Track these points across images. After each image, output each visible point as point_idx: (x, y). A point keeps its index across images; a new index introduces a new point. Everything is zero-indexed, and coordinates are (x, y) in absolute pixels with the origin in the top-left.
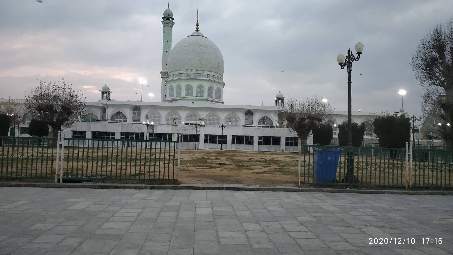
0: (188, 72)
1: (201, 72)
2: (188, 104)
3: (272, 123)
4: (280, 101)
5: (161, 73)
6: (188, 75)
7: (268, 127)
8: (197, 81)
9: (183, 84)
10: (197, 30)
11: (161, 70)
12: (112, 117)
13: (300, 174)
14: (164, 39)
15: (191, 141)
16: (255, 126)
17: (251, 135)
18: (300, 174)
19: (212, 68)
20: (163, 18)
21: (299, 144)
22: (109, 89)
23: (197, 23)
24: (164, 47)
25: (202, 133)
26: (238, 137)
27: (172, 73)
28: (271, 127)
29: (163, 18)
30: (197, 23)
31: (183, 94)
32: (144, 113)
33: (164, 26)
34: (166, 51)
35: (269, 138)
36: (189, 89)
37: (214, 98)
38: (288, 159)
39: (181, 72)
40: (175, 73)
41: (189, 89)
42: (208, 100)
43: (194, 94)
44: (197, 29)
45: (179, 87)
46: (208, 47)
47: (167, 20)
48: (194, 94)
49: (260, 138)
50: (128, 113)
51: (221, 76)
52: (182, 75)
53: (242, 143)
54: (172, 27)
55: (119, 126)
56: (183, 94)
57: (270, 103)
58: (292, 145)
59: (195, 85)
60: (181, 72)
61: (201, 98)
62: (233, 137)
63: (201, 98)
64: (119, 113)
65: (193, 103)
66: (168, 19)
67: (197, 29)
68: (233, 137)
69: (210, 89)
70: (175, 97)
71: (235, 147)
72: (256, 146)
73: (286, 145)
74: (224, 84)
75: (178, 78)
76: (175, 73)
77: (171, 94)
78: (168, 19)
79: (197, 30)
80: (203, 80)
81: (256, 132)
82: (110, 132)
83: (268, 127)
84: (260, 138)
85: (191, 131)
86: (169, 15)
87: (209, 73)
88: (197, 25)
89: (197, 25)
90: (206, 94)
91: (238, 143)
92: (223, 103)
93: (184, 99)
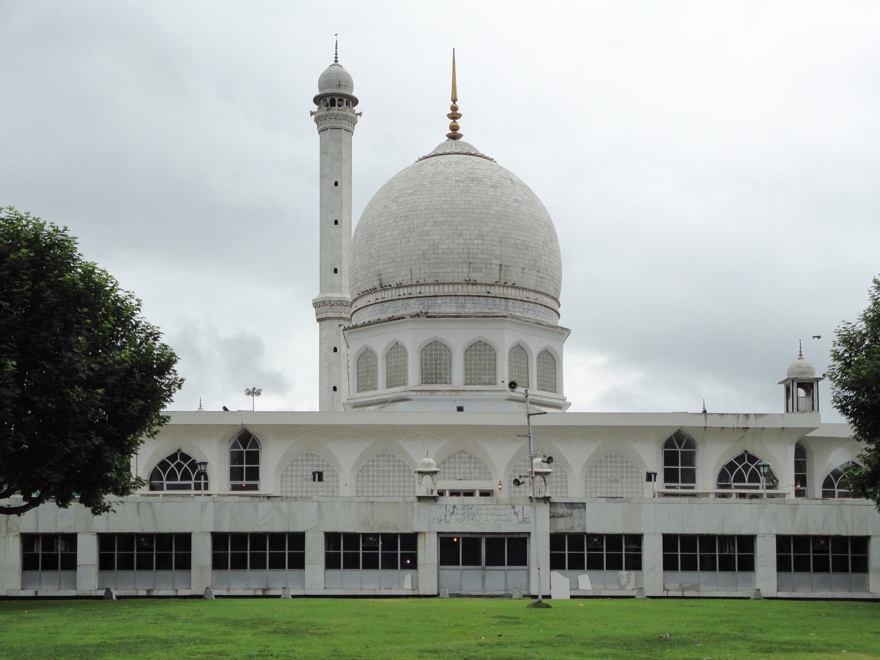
2: (439, 413)
3: (772, 480)
4: (802, 392)
5: (317, 305)
11: (315, 293)
12: (155, 475)
14: (322, 177)
15: (495, 560)
16: (707, 495)
17: (745, 531)
20: (317, 100)
21: (759, 562)
23: (454, 109)
24: (325, 205)
26: (689, 541)
29: (317, 100)
30: (454, 109)
33: (321, 131)
34: (333, 222)
44: (454, 128)
50: (217, 461)
53: (708, 566)
54: (351, 132)
55: (203, 506)
57: (175, 396)
58: (50, 564)
62: (219, 539)
64: (178, 457)
65: (460, 409)
66: (335, 102)
67: (454, 128)
68: (219, 539)
69: (519, 351)
70: (382, 391)
71: (560, 585)
72: (652, 573)
77: (365, 380)
78: (335, 102)
79: (454, 135)
81: (656, 516)
82: (395, 535)
89: (454, 115)
91: (689, 565)
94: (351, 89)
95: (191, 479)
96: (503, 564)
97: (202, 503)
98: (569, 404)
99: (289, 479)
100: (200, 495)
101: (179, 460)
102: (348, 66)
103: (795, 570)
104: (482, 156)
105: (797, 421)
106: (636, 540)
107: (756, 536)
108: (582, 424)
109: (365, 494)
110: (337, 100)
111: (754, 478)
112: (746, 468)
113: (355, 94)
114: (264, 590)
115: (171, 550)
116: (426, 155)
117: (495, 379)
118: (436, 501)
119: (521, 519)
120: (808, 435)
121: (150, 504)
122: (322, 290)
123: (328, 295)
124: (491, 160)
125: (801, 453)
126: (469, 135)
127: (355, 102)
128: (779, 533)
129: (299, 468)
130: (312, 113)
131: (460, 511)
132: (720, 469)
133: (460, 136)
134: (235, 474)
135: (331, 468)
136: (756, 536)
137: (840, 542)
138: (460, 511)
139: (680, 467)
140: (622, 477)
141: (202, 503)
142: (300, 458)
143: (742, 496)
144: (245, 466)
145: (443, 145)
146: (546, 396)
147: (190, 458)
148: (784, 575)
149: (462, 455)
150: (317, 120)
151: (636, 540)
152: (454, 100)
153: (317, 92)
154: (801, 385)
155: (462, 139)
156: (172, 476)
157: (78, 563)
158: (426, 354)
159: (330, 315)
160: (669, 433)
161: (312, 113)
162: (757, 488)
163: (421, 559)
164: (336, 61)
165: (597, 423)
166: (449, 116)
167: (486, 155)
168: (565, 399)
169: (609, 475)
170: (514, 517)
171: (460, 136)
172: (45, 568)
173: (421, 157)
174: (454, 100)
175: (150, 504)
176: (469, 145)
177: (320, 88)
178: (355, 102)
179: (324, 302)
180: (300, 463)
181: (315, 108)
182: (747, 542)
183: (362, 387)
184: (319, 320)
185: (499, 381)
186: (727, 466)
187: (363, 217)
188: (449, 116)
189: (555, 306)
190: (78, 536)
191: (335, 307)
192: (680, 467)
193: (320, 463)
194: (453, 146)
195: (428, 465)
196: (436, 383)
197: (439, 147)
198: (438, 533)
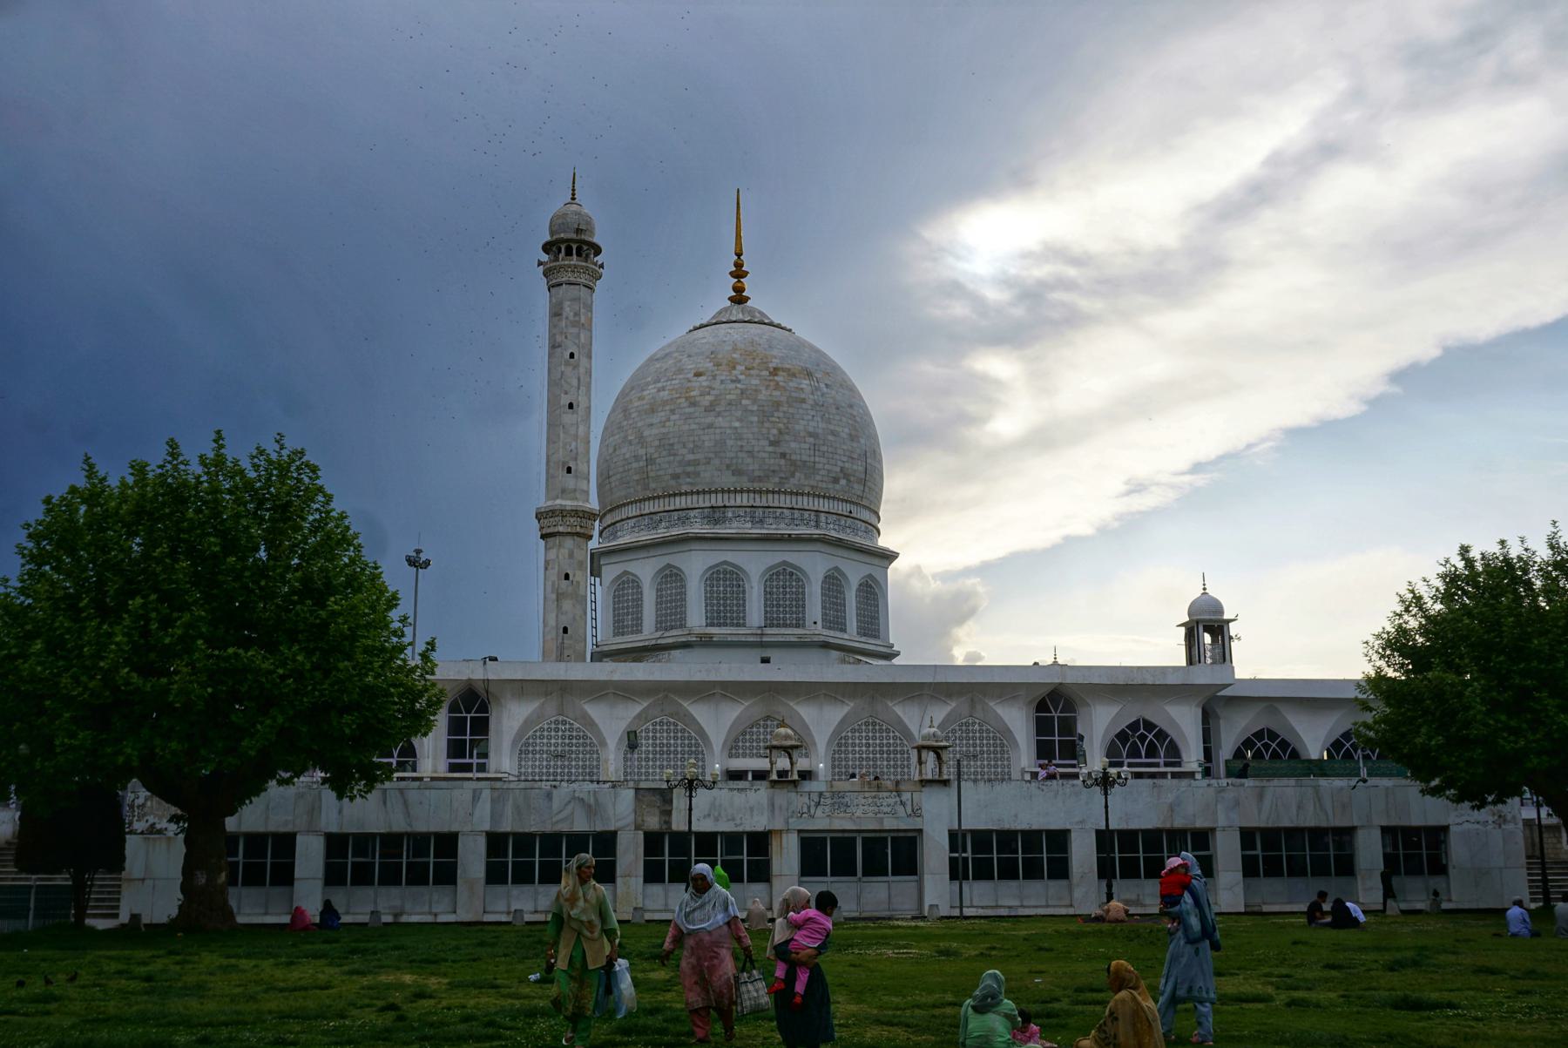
1: (786, 501)
2: (743, 668)
3: (1174, 752)
4: (1207, 638)
6: (715, 514)
7: (1163, 775)
8: (768, 546)
10: (739, 298)
15: (874, 868)
19: (836, 480)
20: (547, 248)
22: (1218, 608)
23: (739, 265)
25: (936, 819)
27: (632, 511)
28: (1174, 775)
29: (547, 248)
30: (739, 265)
31: (696, 618)
32: (509, 720)
35: (1007, 838)
36: (725, 583)
37: (851, 635)
38: (304, 972)
39: (680, 502)
40: (649, 507)
41: (725, 588)
42: (826, 646)
44: (739, 290)
45: (672, 578)
46: (809, 375)
47: (569, 253)
49: (1248, 836)
51: (865, 515)
52: (684, 521)
56: (696, 618)
59: (755, 564)
60: (680, 502)
63: (791, 634)
65: (765, 661)
67: (739, 290)
69: (833, 583)
70: (648, 632)
72: (936, 888)
73: (954, 876)
74: (889, 556)
75: (662, 532)
76: (649, 507)
79: (739, 298)
80: (799, 539)
83: (1163, 775)
84: (1248, 836)
85: (864, 814)
86: (578, 231)
87: (824, 505)
88: (739, 273)
89: (739, 273)
90: (814, 609)
94: (592, 233)
96: (886, 874)
97: (475, 791)
98: (897, 654)
102: (589, 206)
103: (1265, 875)
104: (778, 326)
105: (1204, 675)
106: (1345, 834)
107: (1213, 830)
108: (865, 680)
111: (1152, 751)
112: (1143, 738)
113: (596, 240)
114: (396, 915)
115: (506, 856)
116: (704, 322)
119: (909, 811)
120: (1222, 693)
121: (401, 791)
125: (1208, 717)
126: (757, 300)
127: (598, 251)
128: (1245, 825)
130: (540, 263)
131: (829, 801)
132: (1108, 741)
136: (1213, 830)
137: (1031, 838)
138: (829, 801)
140: (982, 752)
141: (475, 791)
143: (1138, 776)
145: (726, 309)
146: (871, 645)
148: (1253, 881)
151: (1345, 834)
152: (739, 255)
154: (1207, 629)
157: (297, 875)
159: (561, 529)
160: (1043, 692)
161: (540, 263)
162: (1157, 765)
163: (776, 868)
165: (928, 679)
170: (900, 809)
172: (355, 882)
174: (739, 255)
175: (401, 791)
177: (552, 233)
178: (598, 251)
181: (545, 257)
182: (1059, 840)
183: (619, 628)
185: (809, 622)
187: (622, 405)
189: (873, 520)
190: (299, 838)
195: (787, 737)
197: (720, 313)
198: (799, 831)
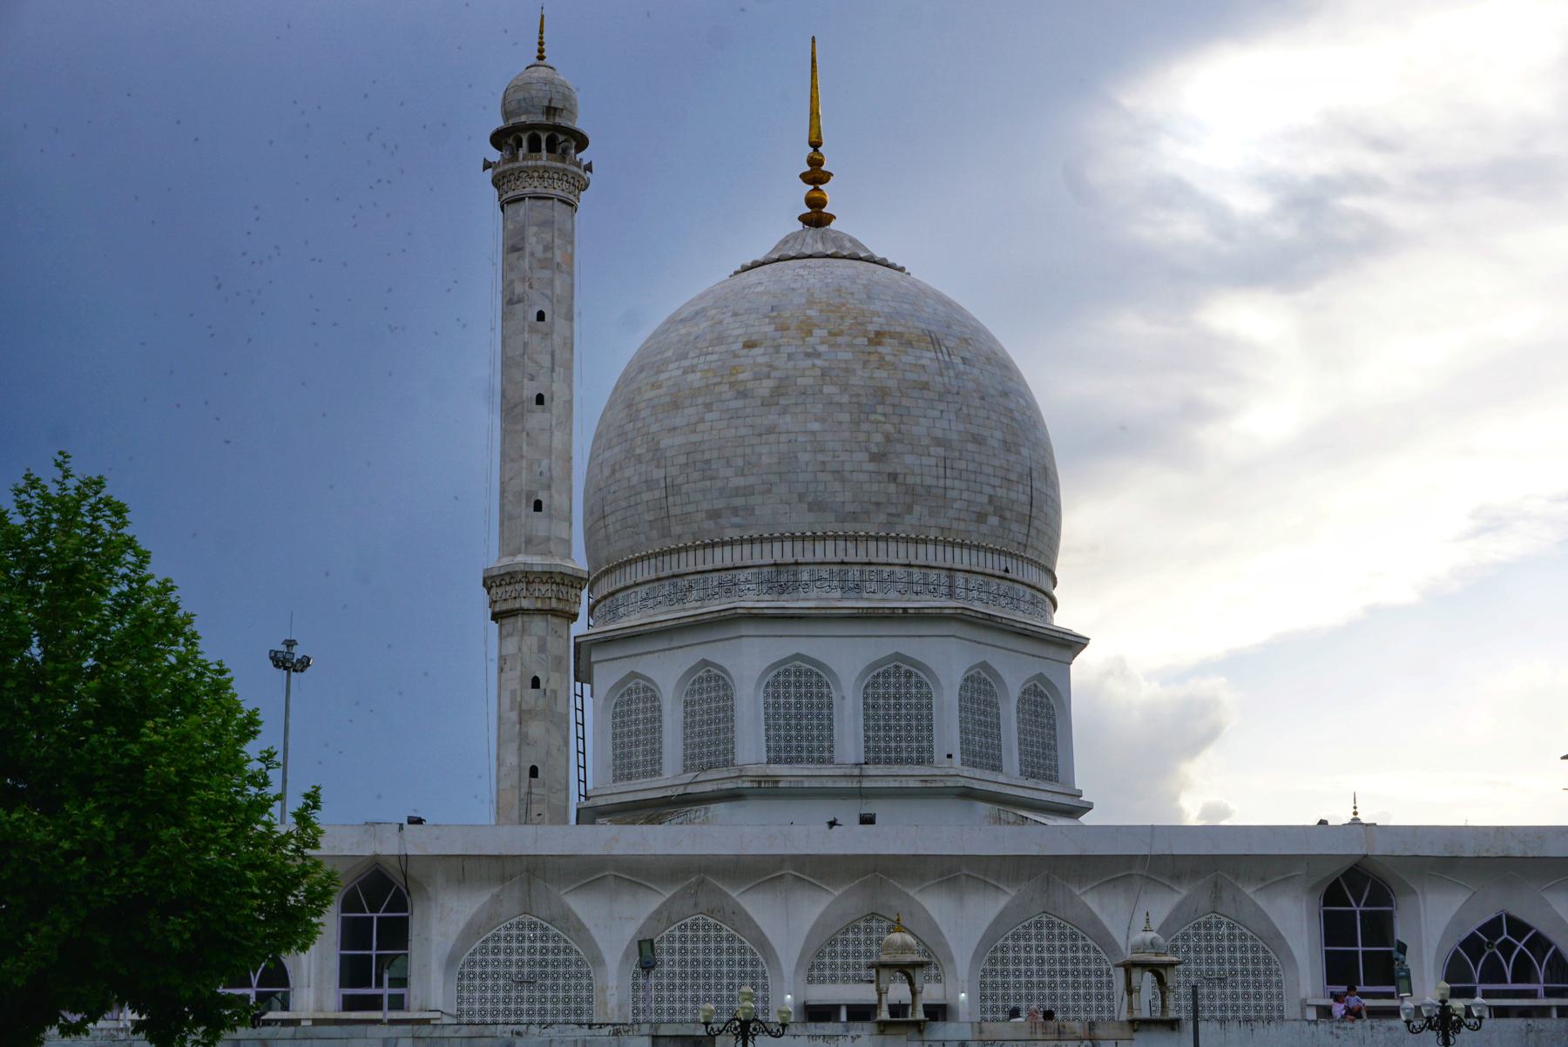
0: (779, 553)
2: (800, 832)
6: (781, 576)
7: (1543, 1012)
8: (870, 629)
9: (749, 661)
10: (816, 217)
13: (543, 146)
18: (543, 146)
19: (981, 518)
20: (498, 139)
23: (815, 162)
29: (498, 139)
30: (815, 162)
31: (750, 749)
37: (1010, 777)
39: (722, 557)
41: (799, 697)
42: (968, 794)
43: (849, 741)
44: (816, 203)
45: (711, 685)
46: (936, 343)
47: (534, 147)
48: (849, 741)
52: (729, 588)
56: (750, 749)
59: (847, 659)
60: (722, 557)
61: (909, 775)
63: (909, 775)
65: (867, 820)
67: (816, 203)
69: (980, 690)
70: (672, 775)
74: (1073, 644)
75: (692, 608)
79: (816, 217)
83: (1543, 1012)
86: (550, 110)
87: (963, 559)
89: (816, 175)
90: (948, 733)
92: (1076, 810)
93: (767, 790)
94: (573, 114)
95: (249, 985)
99: (477, 982)
100: (379, 1022)
101: (1505, 935)
102: (566, 70)
109: (678, 1017)
110: (544, 137)
112: (1507, 948)
113: (580, 124)
116: (760, 257)
117: (930, 750)
118: (921, 1031)
122: (506, 548)
123: (520, 558)
124: (902, 269)
126: (851, 218)
129: (502, 957)
133: (830, 218)
134: (1338, 970)
135: (573, 957)
139: (1360, 948)
142: (503, 933)
143: (1501, 1012)
144: (374, 952)
146: (1044, 792)
147: (1528, 928)
149: (874, 924)
150: (497, 182)
152: (816, 145)
153: (499, 123)
155: (833, 225)
156: (1493, 973)
158: (776, 696)
159: (525, 604)
160: (1335, 870)
162: (1532, 994)
164: (541, 58)
166: (804, 177)
167: (890, 261)
168: (1079, 795)
169: (1204, 967)
171: (830, 218)
173: (748, 262)
174: (816, 145)
176: (852, 240)
177: (506, 115)
178: (582, 142)
179: (512, 575)
180: (502, 944)
181: (495, 155)
183: (623, 768)
184: (496, 617)
185: (939, 755)
186: (1463, 944)
188: (804, 177)
189: (1045, 583)
191: (536, 586)
192: (374, 952)
193: (550, 945)
194: (813, 241)
195: (905, 948)
196: (799, 760)
